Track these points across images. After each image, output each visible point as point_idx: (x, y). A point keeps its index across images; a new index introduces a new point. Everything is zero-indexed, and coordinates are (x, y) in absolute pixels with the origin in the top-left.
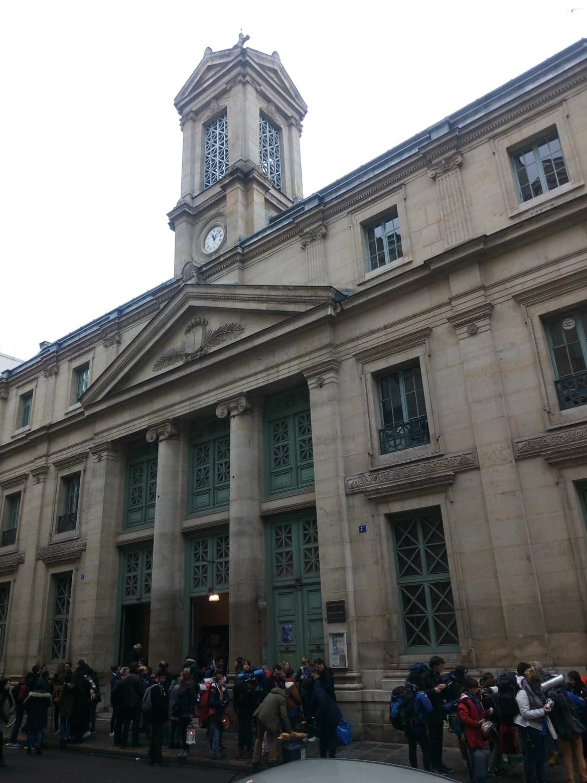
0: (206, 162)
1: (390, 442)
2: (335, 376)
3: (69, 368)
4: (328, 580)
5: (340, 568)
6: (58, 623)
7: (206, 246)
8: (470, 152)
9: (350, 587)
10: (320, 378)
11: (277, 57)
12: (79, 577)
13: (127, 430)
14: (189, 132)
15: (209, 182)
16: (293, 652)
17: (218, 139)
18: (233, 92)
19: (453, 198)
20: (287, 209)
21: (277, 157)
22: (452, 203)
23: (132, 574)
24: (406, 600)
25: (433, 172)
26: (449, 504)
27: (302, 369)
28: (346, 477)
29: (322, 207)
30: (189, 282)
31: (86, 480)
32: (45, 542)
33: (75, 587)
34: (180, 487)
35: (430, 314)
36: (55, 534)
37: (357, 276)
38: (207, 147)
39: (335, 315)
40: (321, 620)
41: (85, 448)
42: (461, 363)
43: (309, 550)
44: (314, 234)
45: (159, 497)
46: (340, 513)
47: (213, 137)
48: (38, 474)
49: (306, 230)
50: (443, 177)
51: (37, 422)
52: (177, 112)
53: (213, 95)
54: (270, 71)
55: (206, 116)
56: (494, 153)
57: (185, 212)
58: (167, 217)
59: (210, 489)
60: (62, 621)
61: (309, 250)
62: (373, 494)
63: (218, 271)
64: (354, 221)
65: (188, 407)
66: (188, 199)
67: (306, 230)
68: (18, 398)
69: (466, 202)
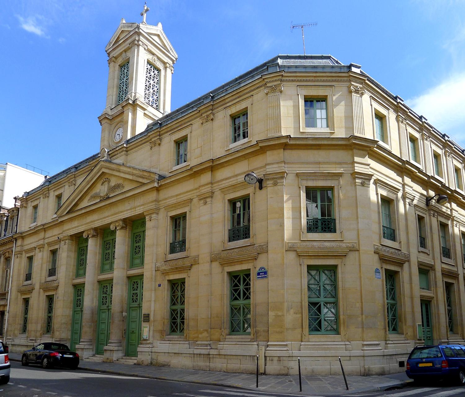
2: (157, 216)
3: (54, 195)
4: (145, 305)
7: (116, 137)
9: (152, 309)
16: (135, 333)
23: (135, 292)
24: (172, 314)
26: (188, 277)
27: (144, 211)
28: (156, 263)
29: (159, 130)
32: (43, 281)
33: (55, 302)
34: (97, 260)
35: (192, 192)
39: (158, 187)
46: (152, 278)
48: (40, 248)
51: (194, 159)
53: (123, 49)
55: (120, 61)
65: (100, 223)
68: (32, 207)
69: (212, 139)
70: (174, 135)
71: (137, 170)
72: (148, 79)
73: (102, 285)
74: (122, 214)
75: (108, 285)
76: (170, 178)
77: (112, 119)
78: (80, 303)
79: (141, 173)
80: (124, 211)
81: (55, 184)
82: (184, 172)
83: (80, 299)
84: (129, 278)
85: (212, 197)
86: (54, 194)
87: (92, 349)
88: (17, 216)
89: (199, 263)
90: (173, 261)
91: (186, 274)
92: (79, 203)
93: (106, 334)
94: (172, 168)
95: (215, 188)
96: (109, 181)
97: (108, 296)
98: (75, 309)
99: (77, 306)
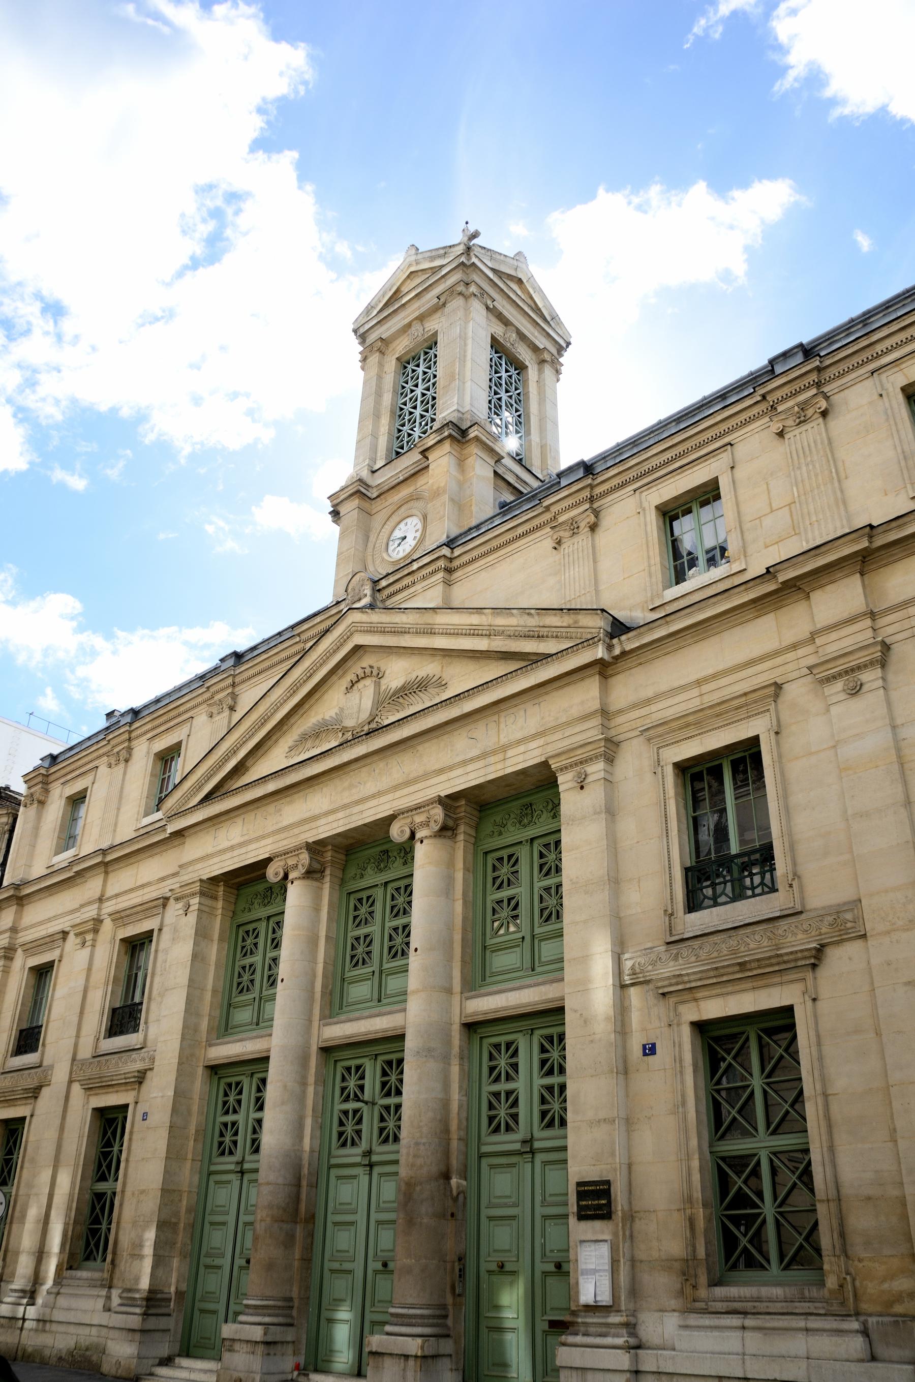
0: (400, 416)
1: (704, 890)
3: (148, 753)
5: (605, 1120)
6: (100, 1196)
8: (842, 394)
10: (580, 773)
11: (522, 259)
12: (139, 1117)
13: (236, 860)
14: (374, 371)
15: (402, 448)
17: (420, 380)
18: (450, 307)
19: (814, 466)
20: (529, 489)
21: (517, 411)
22: (812, 473)
24: (723, 1182)
25: (780, 425)
27: (547, 755)
30: (355, 606)
31: (162, 946)
32: (85, 1052)
33: (131, 1133)
35: (779, 660)
36: (104, 1038)
37: (649, 595)
38: (402, 394)
39: (611, 660)
40: (566, 1216)
41: (163, 889)
42: (834, 746)
43: (550, 1089)
44: (576, 526)
45: (282, 980)
47: (412, 378)
49: (562, 519)
50: (797, 432)
52: (357, 341)
53: (417, 314)
54: (512, 280)
55: (402, 346)
56: (881, 395)
57: (358, 491)
58: (329, 501)
59: (523, 938)
60: (105, 1193)
61: (566, 551)
62: (671, 985)
63: (407, 587)
64: (645, 505)
66: (365, 474)
67: (562, 519)
68: (63, 801)
70: (654, 489)
71: (513, 615)
72: (494, 387)
73: (340, 1065)
74: (443, 778)
75: (368, 1065)
76: (667, 622)
77: (378, 496)
78: (234, 1138)
79: (532, 622)
80: (451, 768)
81: (155, 715)
82: (732, 592)
83: (234, 1124)
84: (471, 1027)
85: (883, 663)
86: (149, 749)
87: (293, 1342)
88: (7, 836)
89: (864, 936)
90: (715, 938)
91: (797, 988)
92: (248, 764)
93: (359, 1274)
94: (660, 596)
95: (890, 630)
96: (380, 676)
97: (366, 1109)
98: (210, 1162)
99: (223, 1154)
